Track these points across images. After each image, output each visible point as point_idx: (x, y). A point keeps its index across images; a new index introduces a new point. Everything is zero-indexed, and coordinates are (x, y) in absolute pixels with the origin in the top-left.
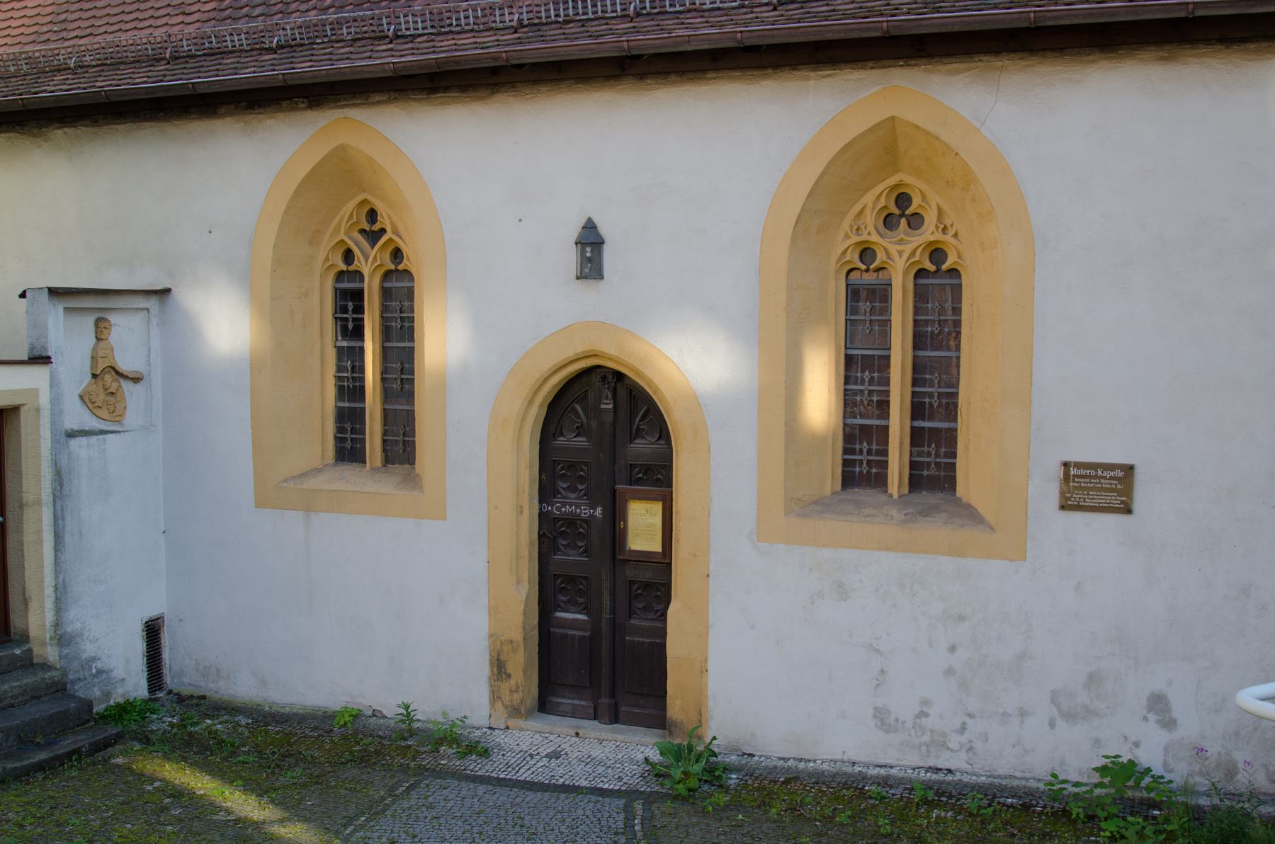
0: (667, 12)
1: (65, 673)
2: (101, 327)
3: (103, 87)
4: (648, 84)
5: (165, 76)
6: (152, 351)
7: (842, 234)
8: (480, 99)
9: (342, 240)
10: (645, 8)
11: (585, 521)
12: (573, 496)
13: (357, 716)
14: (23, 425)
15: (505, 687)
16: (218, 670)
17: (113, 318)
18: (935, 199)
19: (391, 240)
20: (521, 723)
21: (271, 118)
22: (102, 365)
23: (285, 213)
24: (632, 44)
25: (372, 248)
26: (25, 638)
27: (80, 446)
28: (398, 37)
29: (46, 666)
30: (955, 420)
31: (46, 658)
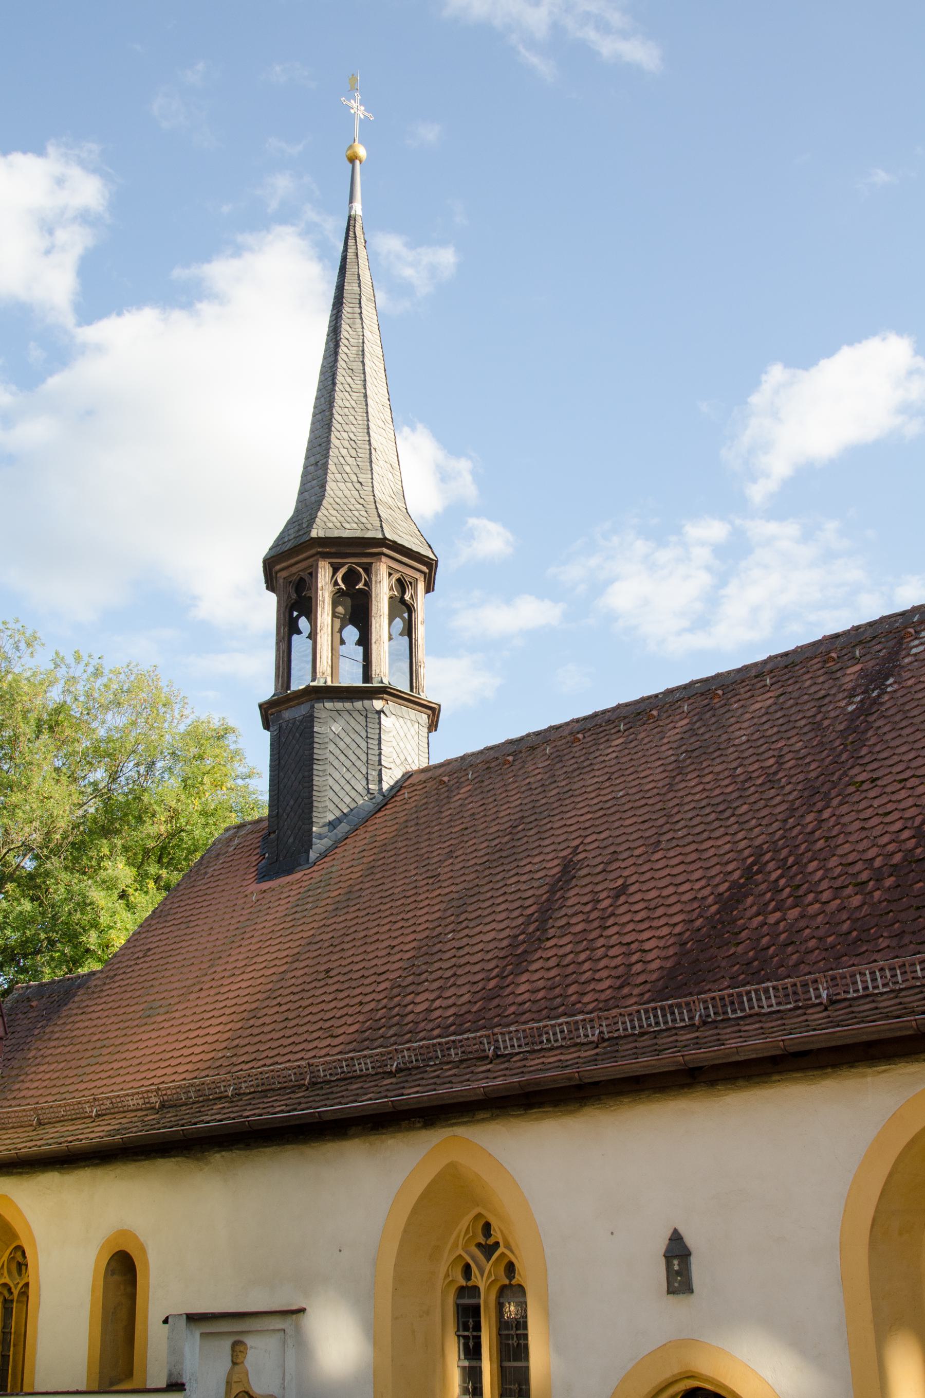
0: (730, 1019)
2: (238, 1349)
3: (248, 1117)
4: (719, 1090)
5: (300, 1103)
6: (286, 1374)
8: (571, 1112)
9: (460, 1255)
10: (709, 1016)
17: (250, 1341)
19: (503, 1254)
21: (391, 1138)
23: (405, 1231)
24: (687, 1058)
25: (488, 1260)
28: (498, 1056)
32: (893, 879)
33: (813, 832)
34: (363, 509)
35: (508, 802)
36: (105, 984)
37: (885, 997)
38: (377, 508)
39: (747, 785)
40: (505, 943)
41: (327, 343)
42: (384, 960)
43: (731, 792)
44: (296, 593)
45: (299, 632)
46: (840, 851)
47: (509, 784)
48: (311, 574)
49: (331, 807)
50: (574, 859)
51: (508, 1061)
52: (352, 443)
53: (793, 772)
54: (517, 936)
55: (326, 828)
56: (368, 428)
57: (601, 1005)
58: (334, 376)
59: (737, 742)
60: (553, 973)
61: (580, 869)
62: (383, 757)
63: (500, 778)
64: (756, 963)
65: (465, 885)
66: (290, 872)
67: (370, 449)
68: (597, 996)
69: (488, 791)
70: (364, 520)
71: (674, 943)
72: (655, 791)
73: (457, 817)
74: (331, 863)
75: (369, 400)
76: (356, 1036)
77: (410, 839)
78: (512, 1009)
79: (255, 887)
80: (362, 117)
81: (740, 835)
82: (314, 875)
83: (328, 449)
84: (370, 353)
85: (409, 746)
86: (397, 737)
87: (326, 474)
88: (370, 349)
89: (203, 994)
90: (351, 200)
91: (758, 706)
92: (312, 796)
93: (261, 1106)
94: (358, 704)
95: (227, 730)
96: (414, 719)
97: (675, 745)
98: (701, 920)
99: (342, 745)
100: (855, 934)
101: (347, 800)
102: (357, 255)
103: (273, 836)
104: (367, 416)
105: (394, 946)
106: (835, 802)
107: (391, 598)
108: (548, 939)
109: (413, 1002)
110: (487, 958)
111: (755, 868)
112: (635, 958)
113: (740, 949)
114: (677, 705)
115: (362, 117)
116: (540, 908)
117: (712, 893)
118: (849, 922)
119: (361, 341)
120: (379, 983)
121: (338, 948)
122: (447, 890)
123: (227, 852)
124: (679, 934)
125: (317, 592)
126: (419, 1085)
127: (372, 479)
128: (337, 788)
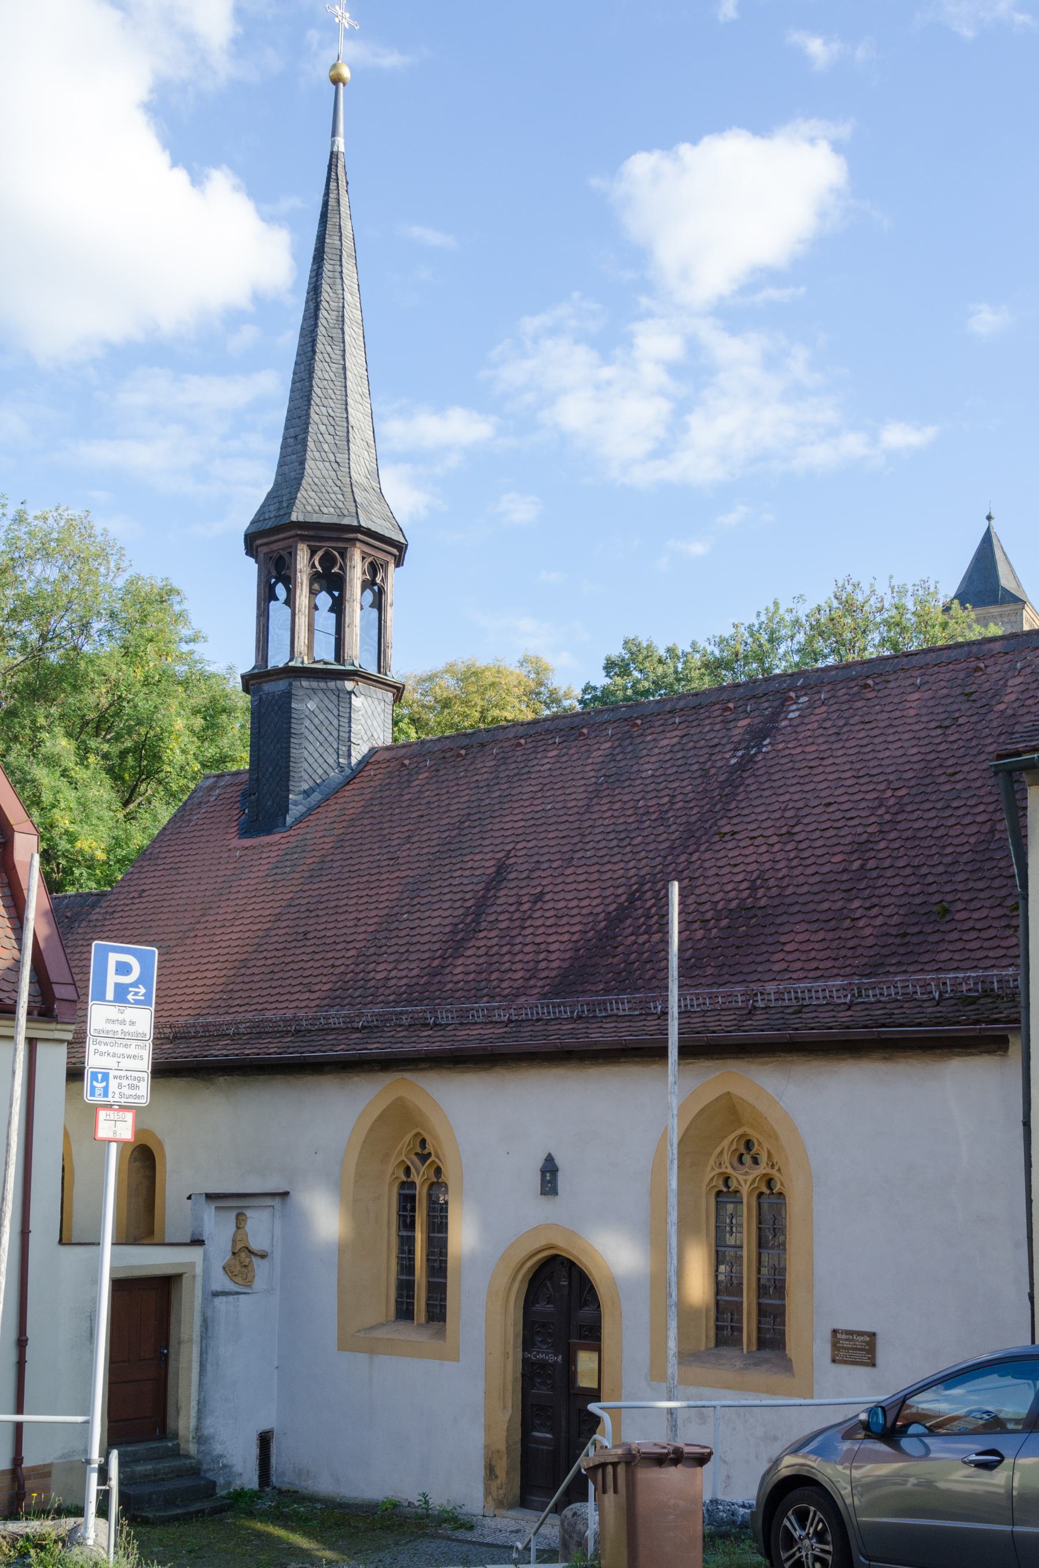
1: (200, 1463)
2: (240, 1219)
3: (248, 1055)
5: (289, 1047)
7: (709, 1168)
11: (551, 1365)
12: (545, 1347)
13: (396, 1505)
14: (184, 1286)
15: (494, 1485)
16: (308, 1472)
17: (249, 1213)
18: (766, 1145)
19: (433, 1162)
20: (504, 1512)
22: (239, 1246)
25: (423, 1165)
26: (176, 1436)
27: (221, 1303)
29: (188, 1456)
30: (784, 1299)
31: (189, 1452)
32: (727, 920)
33: (683, 871)
34: (340, 492)
35: (459, 796)
36: (105, 919)
37: (697, 1015)
38: (353, 492)
39: (645, 818)
40: (448, 929)
41: (307, 302)
42: (352, 930)
43: (633, 823)
44: (276, 570)
45: (276, 599)
46: (698, 891)
47: (461, 778)
48: (290, 553)
49: (306, 777)
50: (507, 862)
51: (444, 1029)
52: (331, 419)
53: (679, 813)
54: (457, 925)
55: (302, 796)
56: (346, 404)
57: (514, 992)
58: (314, 342)
59: (644, 775)
60: (481, 960)
61: (510, 872)
62: (352, 735)
63: (453, 770)
64: (624, 974)
65: (419, 871)
66: (269, 832)
67: (348, 427)
68: (512, 983)
69: (443, 782)
70: (340, 505)
71: (571, 949)
72: (576, 810)
73: (415, 803)
74: (306, 830)
75: (348, 373)
76: (329, 993)
77: (375, 818)
78: (450, 986)
79: (236, 842)
80: (347, 26)
81: (632, 864)
82: (291, 839)
83: (307, 424)
84: (350, 319)
85: (375, 723)
86: (366, 716)
87: (305, 451)
88: (350, 313)
89: (198, 940)
90: (334, 134)
91: (665, 742)
92: (289, 766)
93: (258, 1046)
94: (332, 684)
95: (171, 592)
96: (381, 698)
97: (597, 767)
98: (593, 932)
99: (316, 721)
100: (693, 960)
101: (320, 771)
102: (339, 202)
103: (253, 797)
104: (346, 391)
105: (360, 919)
106: (703, 848)
107: (363, 581)
108: (480, 931)
109: (374, 970)
110: (433, 940)
111: (637, 894)
112: (542, 956)
113: (616, 960)
114: (604, 727)
115: (347, 26)
116: (476, 903)
117: (604, 911)
118: (691, 950)
119: (341, 305)
120: (348, 950)
121: (313, 914)
122: (404, 874)
123: (208, 801)
124: (576, 942)
125: (296, 574)
126: (379, 1042)
127: (349, 459)
128: (311, 760)
